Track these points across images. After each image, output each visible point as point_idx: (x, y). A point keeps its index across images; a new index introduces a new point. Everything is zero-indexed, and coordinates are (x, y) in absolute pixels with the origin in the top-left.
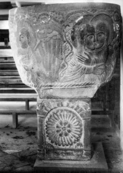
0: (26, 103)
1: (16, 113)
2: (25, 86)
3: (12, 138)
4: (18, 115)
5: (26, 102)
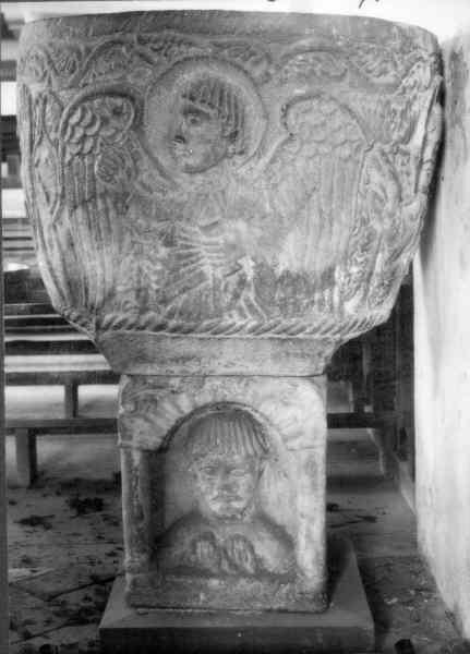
1: (30, 430)
4: (38, 438)
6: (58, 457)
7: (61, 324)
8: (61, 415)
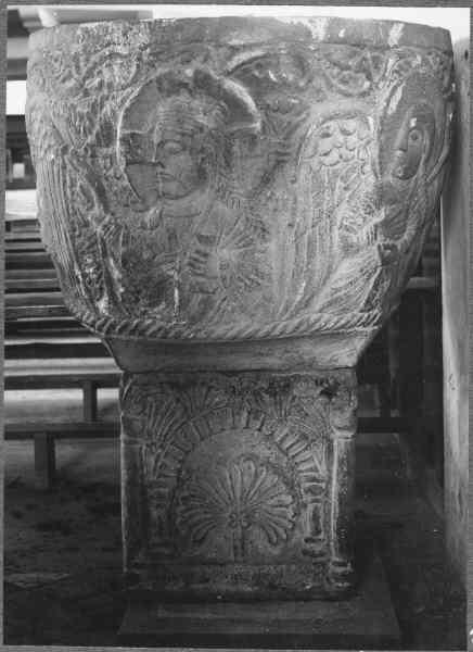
0: (85, 395)
1: (48, 433)
2: (81, 329)
3: (33, 527)
4: (56, 442)
5: (85, 392)
6: (76, 462)
7: (76, 327)
8: (80, 418)
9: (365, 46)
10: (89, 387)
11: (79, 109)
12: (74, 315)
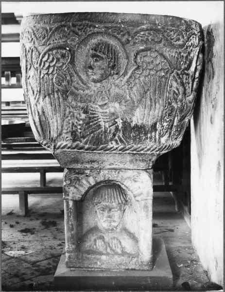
0: (20, 198)
3: (18, 231)
5: (41, 174)
9: (143, 97)
10: (43, 171)
11: (182, 54)
12: (36, 141)
